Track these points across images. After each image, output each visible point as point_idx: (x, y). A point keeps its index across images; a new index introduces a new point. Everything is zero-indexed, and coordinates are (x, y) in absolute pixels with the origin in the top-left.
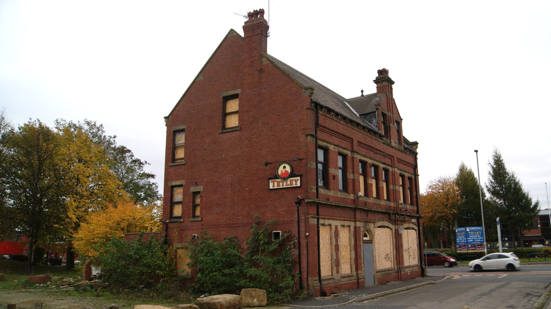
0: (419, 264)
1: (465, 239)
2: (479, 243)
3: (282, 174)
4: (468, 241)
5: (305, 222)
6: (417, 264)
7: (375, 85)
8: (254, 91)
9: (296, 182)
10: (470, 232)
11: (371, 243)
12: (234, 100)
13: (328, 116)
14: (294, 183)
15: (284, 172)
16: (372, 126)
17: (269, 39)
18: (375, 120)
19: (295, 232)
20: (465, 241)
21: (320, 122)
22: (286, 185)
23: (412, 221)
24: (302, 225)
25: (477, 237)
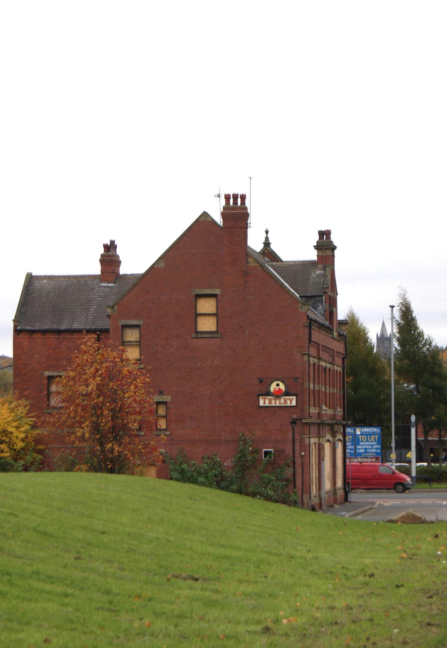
1: (353, 447)
2: (373, 454)
3: (275, 391)
4: (358, 451)
5: (301, 442)
7: (315, 252)
8: (238, 295)
9: (292, 401)
10: (360, 437)
12: (207, 298)
14: (289, 402)
15: (277, 390)
16: (317, 313)
17: (249, 230)
18: (321, 306)
19: (288, 449)
20: (351, 452)
21: (313, 339)
22: (280, 403)
24: (297, 444)
25: (370, 445)
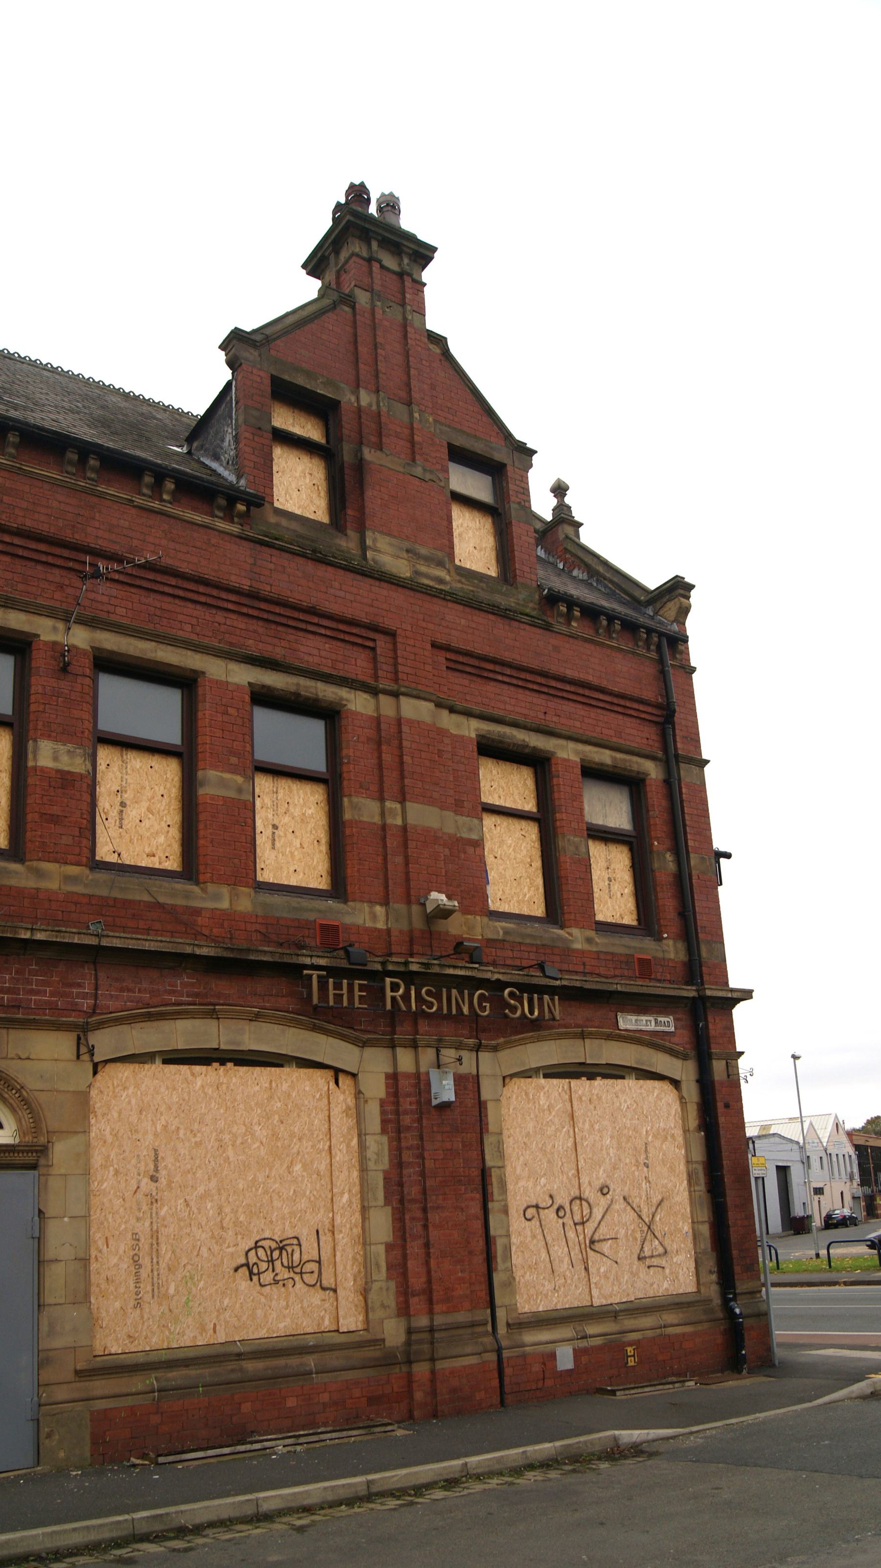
0: (713, 1291)
6: (695, 1290)
11: (34, 1167)
13: (156, 505)
23: (622, 1025)
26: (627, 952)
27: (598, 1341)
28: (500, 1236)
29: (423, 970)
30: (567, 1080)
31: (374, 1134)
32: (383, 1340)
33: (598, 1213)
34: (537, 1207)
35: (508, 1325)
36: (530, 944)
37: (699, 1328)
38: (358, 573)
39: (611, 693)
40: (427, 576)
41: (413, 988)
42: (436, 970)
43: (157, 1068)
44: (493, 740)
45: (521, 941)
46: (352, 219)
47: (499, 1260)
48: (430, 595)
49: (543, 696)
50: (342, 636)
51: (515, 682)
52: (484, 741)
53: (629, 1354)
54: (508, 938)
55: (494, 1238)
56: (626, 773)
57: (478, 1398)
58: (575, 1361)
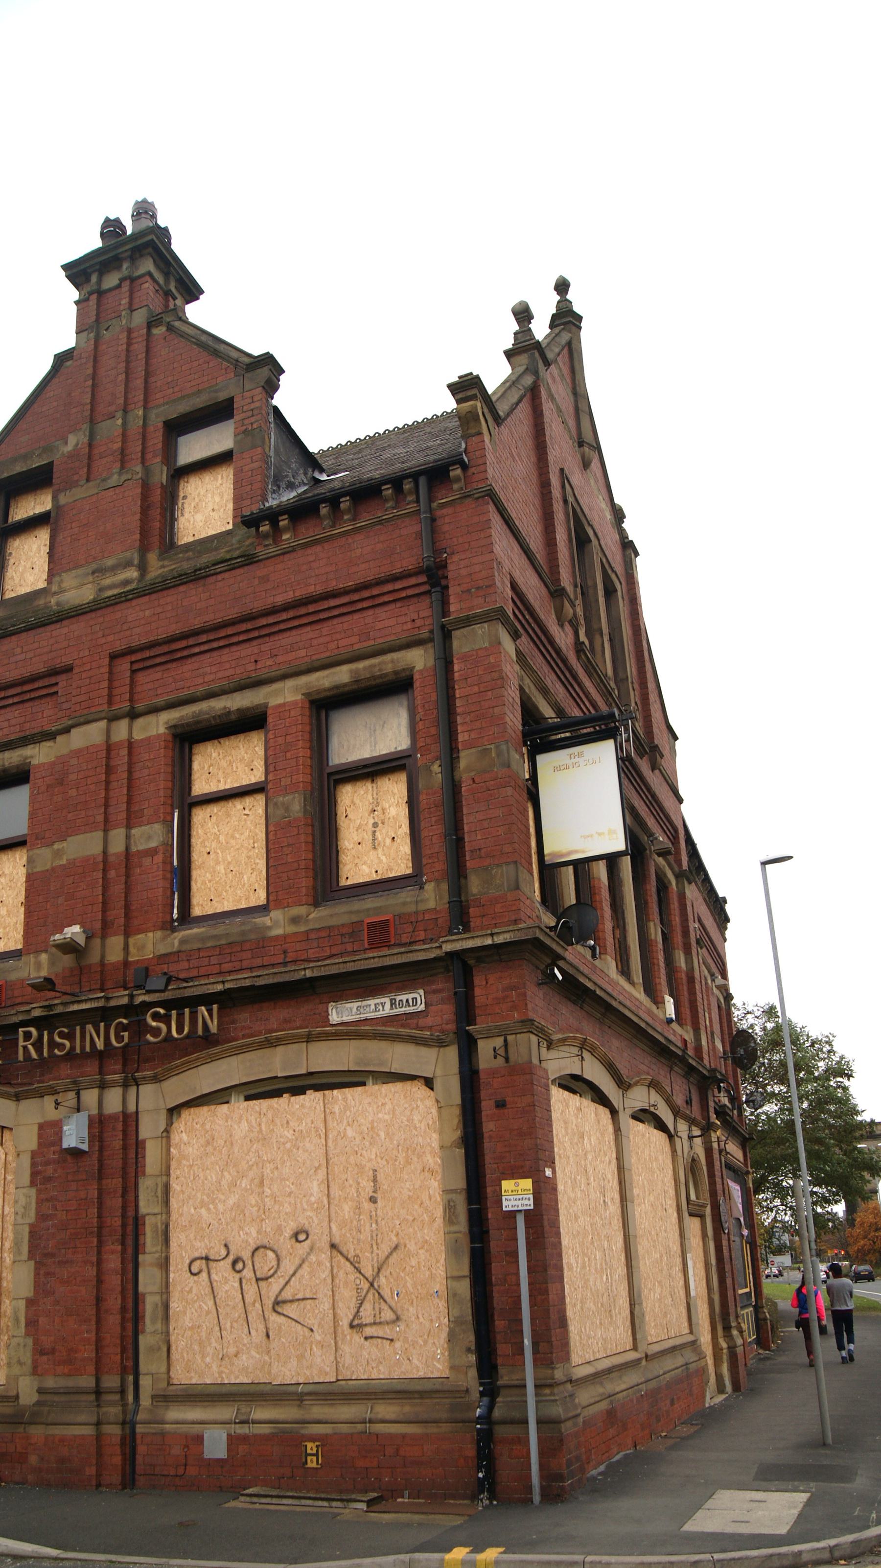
0: (471, 1379)
26: (355, 918)
27: (265, 1429)
28: (151, 1293)
29: (45, 1013)
30: (322, 1092)
31: (24, 1187)
32: (17, 1397)
33: (288, 1266)
34: (207, 1259)
35: (153, 1397)
36: (212, 947)
37: (432, 1429)
38: (40, 627)
39: (346, 592)
40: (110, 587)
41: (46, 1033)
42: (59, 1010)
43: (239, 1106)
44: (188, 724)
45: (200, 946)
46: (155, 239)
47: (148, 1320)
48: (111, 605)
49: (255, 643)
50: (28, 696)
51: (215, 645)
52: (179, 731)
53: (309, 1451)
54: (184, 948)
55: (144, 1295)
56: (379, 681)
57: (87, 1473)
58: (229, 1450)
